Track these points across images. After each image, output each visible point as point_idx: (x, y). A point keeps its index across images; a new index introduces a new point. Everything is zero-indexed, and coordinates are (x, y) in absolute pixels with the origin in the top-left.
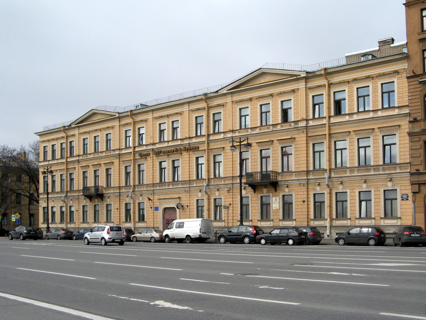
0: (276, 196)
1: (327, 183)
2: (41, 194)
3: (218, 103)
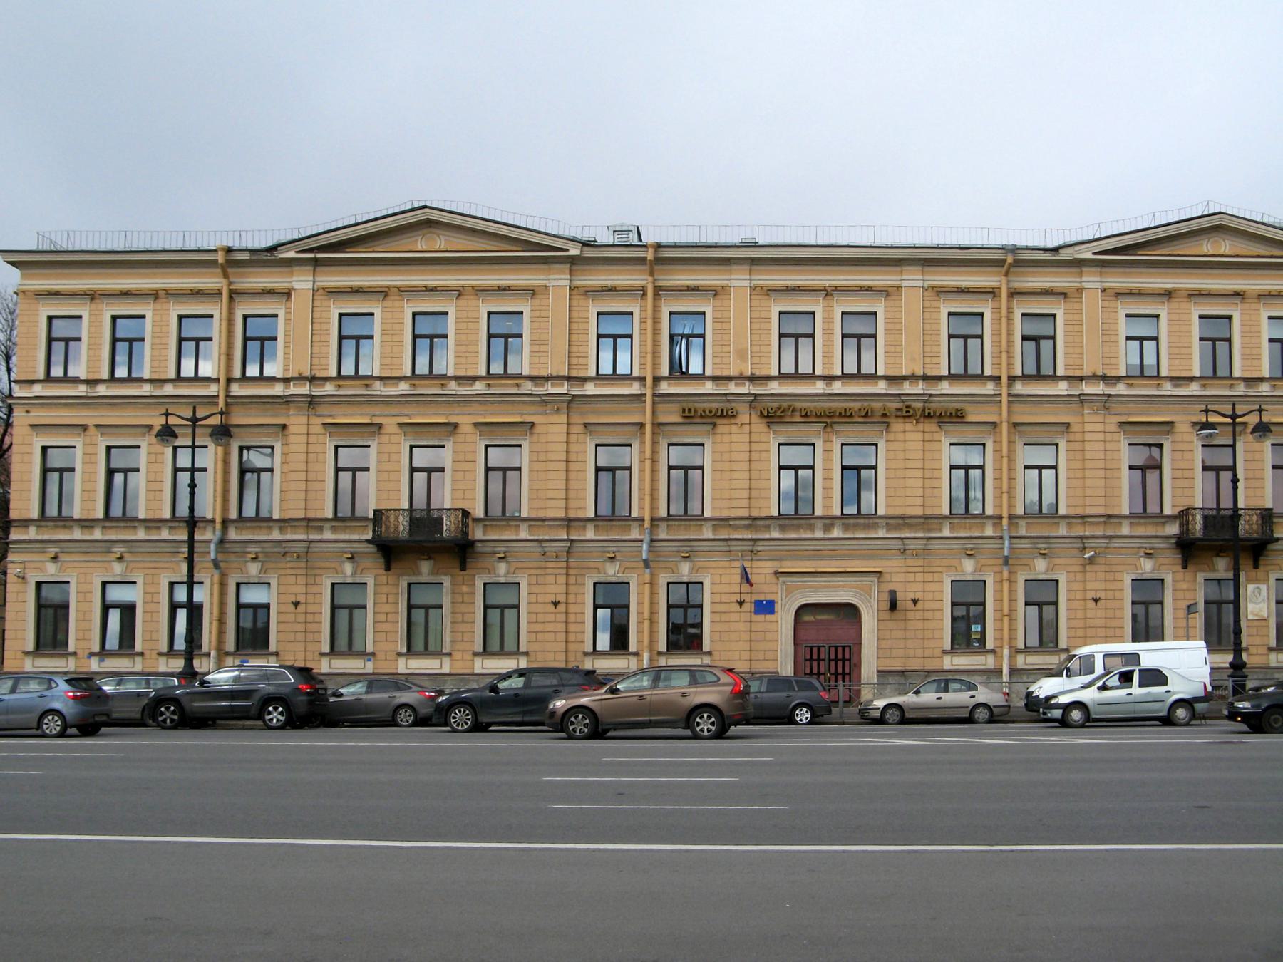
0: (1257, 581)
1: (212, 556)
2: (26, 523)
3: (1049, 285)
